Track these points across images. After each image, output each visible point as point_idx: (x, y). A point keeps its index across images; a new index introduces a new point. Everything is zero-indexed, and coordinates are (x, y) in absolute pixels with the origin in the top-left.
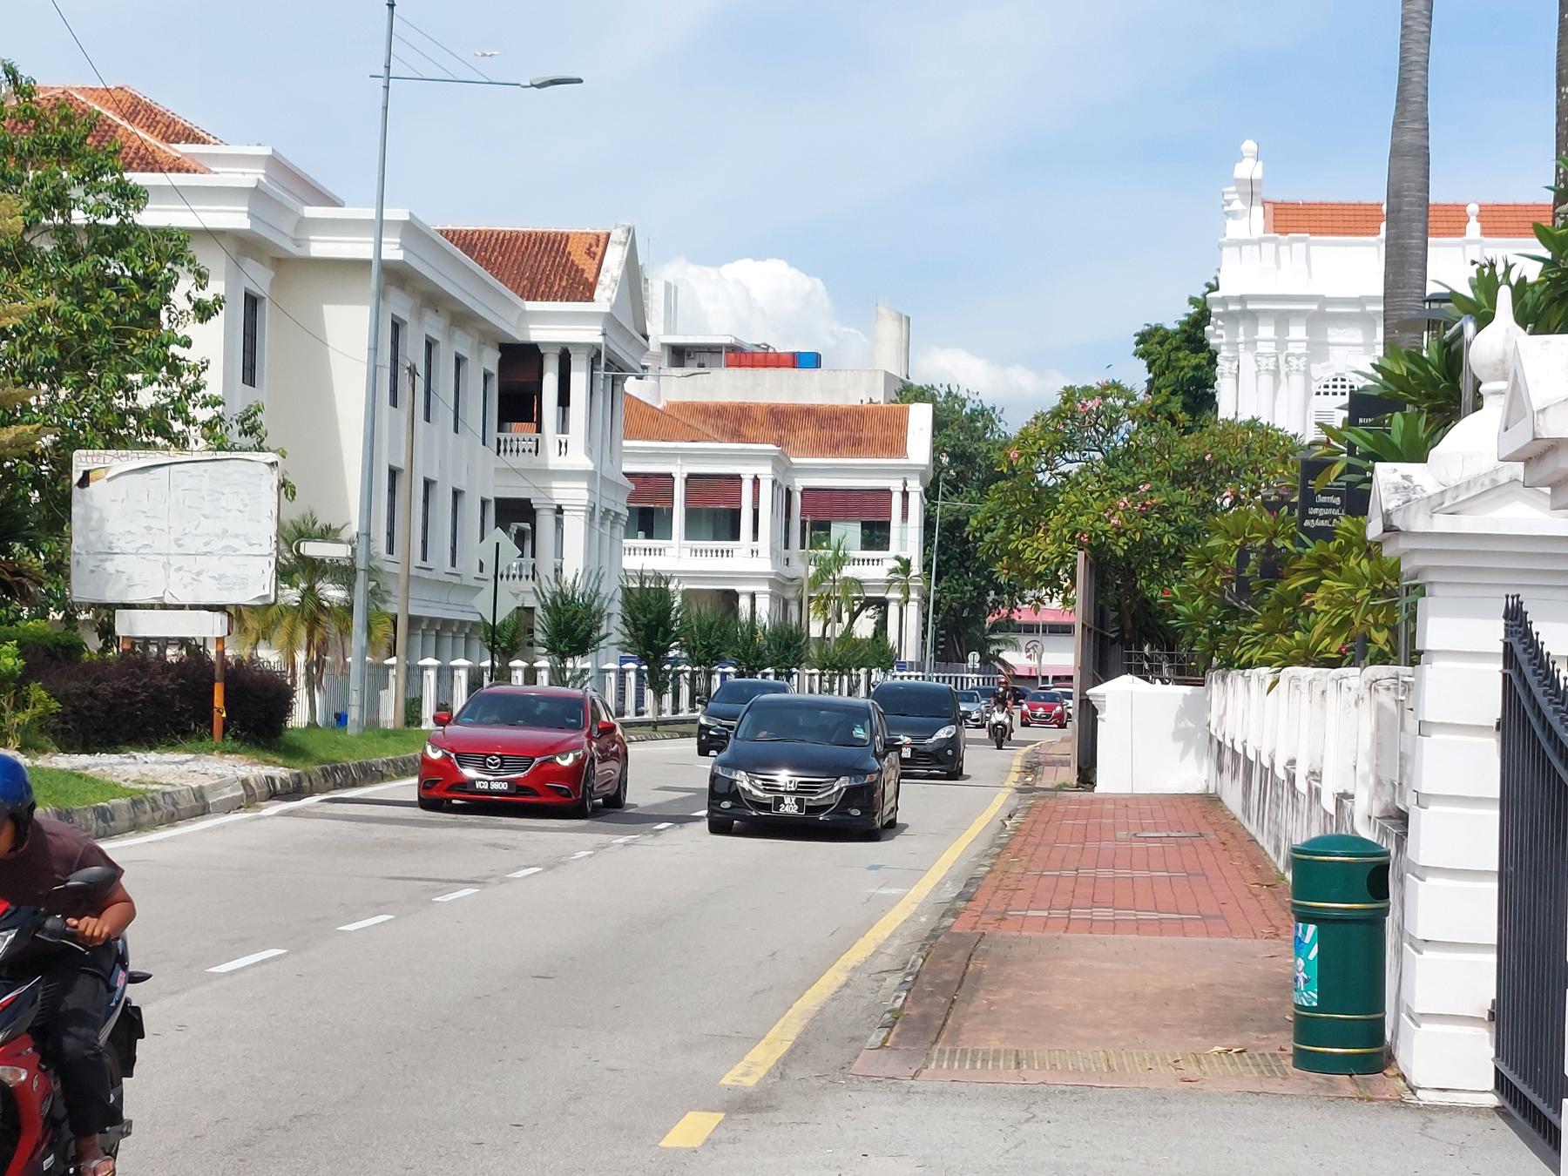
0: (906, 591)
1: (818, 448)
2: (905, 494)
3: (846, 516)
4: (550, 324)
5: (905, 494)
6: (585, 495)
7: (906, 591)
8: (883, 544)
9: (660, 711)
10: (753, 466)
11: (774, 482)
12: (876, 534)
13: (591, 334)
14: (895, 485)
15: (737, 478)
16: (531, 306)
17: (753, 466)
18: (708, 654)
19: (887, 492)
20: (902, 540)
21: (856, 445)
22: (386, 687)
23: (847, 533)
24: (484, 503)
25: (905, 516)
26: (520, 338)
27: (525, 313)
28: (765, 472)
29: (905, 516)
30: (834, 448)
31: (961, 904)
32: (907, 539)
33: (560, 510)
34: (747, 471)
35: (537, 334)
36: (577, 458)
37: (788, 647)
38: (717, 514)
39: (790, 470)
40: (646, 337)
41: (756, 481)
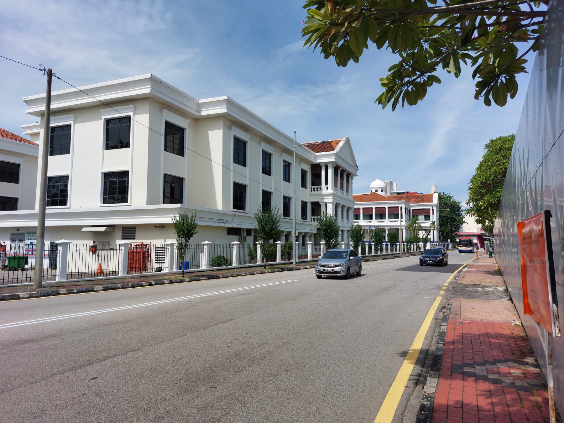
0: (434, 228)
1: (415, 202)
2: (433, 210)
3: (421, 214)
4: (323, 158)
5: (433, 210)
6: (332, 200)
7: (434, 228)
8: (429, 219)
9: (377, 253)
10: (401, 205)
11: (405, 208)
12: (427, 217)
13: (332, 159)
14: (431, 208)
15: (398, 207)
16: (317, 154)
17: (401, 205)
18: (357, 239)
19: (429, 209)
20: (433, 218)
21: (423, 201)
22: (202, 252)
23: (421, 218)
24: (304, 204)
25: (433, 214)
26: (315, 162)
27: (316, 156)
28: (403, 206)
29: (433, 214)
30: (419, 202)
31: (475, 241)
32: (434, 217)
33: (326, 205)
34: (400, 206)
35: (319, 161)
36: (330, 191)
37: (393, 238)
38: (394, 214)
39: (410, 206)
40: (357, 166)
41: (402, 207)
